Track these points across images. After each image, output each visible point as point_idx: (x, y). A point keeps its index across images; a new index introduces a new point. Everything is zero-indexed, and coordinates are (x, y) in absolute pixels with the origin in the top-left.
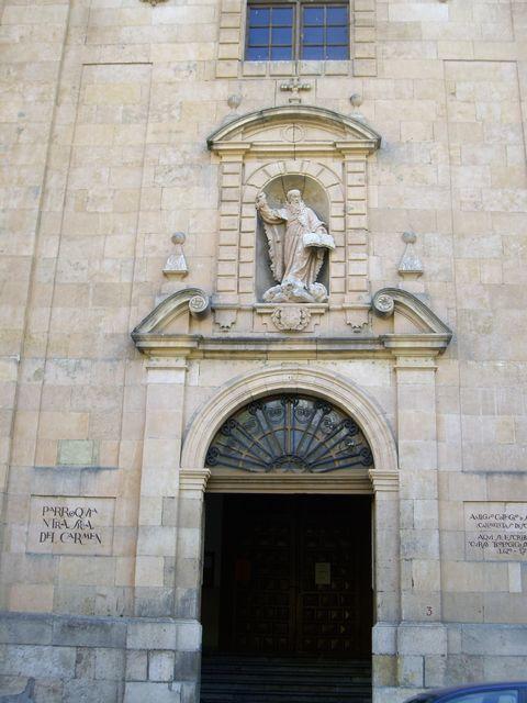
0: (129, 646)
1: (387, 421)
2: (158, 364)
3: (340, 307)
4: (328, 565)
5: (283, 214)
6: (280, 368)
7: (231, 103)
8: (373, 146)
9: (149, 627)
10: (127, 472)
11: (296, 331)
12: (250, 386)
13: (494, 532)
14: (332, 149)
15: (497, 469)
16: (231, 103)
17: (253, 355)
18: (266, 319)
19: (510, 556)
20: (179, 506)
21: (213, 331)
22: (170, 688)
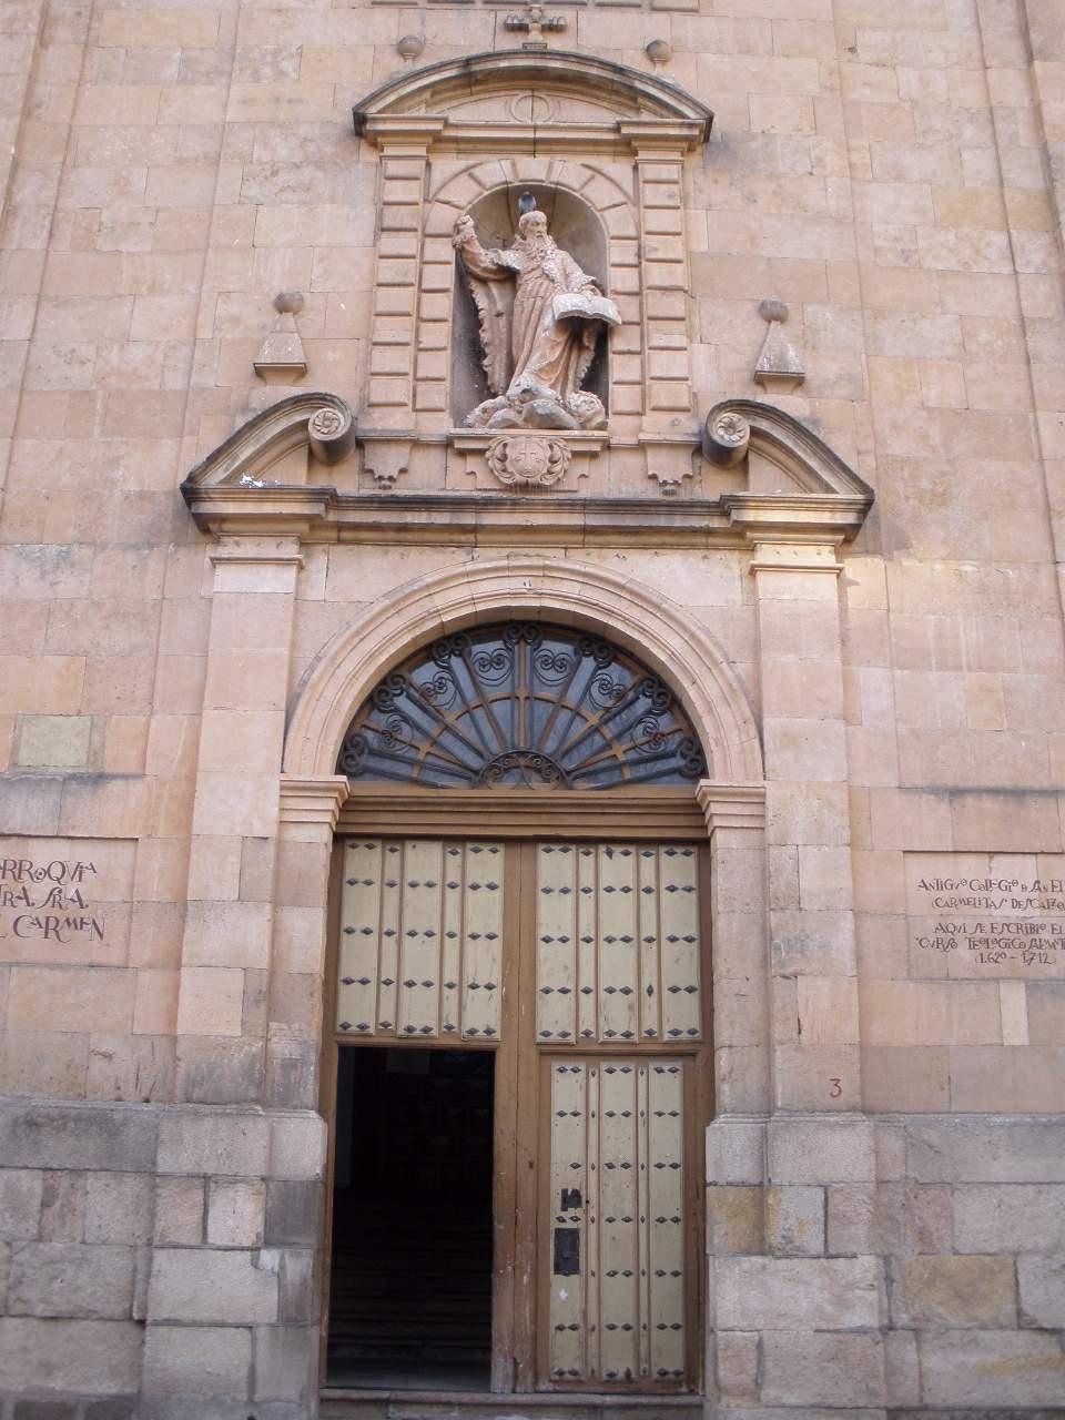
0: (162, 1168)
1: (738, 678)
2: (238, 552)
3: (633, 441)
4: (1027, 1043)
5: (510, 258)
6: (504, 563)
7: (404, 50)
8: (696, 132)
9: (208, 1124)
10: (163, 783)
11: (539, 488)
12: (440, 601)
13: (963, 917)
14: (611, 136)
15: (970, 784)
16: (404, 50)
17: (445, 537)
18: (472, 463)
19: (1003, 968)
20: (278, 858)
21: (360, 487)
22: (255, 1263)
